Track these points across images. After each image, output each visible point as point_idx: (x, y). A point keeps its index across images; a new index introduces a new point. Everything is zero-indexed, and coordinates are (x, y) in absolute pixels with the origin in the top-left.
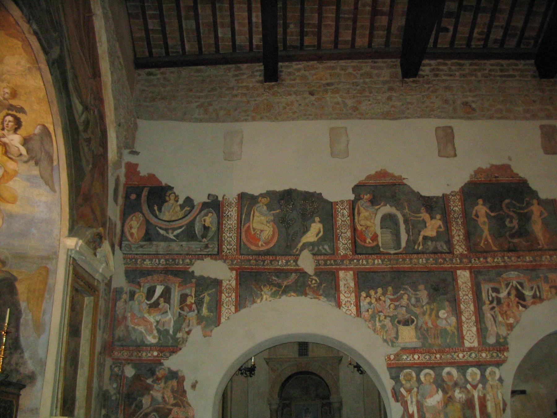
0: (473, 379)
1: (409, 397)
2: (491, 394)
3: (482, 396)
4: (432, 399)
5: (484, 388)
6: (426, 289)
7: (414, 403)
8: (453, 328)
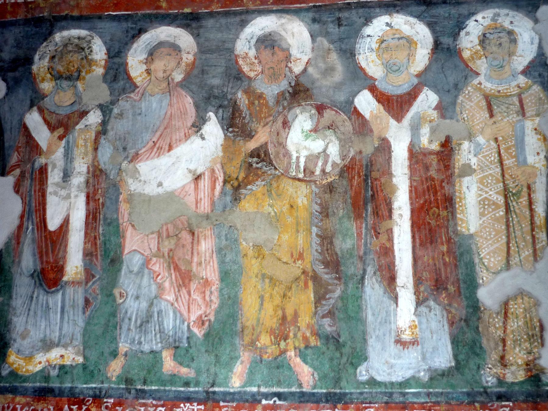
0: (390, 68)
1: (59, 154)
2: (481, 139)
3: (435, 146)
4: (165, 161)
5: (444, 109)
7: (78, 180)
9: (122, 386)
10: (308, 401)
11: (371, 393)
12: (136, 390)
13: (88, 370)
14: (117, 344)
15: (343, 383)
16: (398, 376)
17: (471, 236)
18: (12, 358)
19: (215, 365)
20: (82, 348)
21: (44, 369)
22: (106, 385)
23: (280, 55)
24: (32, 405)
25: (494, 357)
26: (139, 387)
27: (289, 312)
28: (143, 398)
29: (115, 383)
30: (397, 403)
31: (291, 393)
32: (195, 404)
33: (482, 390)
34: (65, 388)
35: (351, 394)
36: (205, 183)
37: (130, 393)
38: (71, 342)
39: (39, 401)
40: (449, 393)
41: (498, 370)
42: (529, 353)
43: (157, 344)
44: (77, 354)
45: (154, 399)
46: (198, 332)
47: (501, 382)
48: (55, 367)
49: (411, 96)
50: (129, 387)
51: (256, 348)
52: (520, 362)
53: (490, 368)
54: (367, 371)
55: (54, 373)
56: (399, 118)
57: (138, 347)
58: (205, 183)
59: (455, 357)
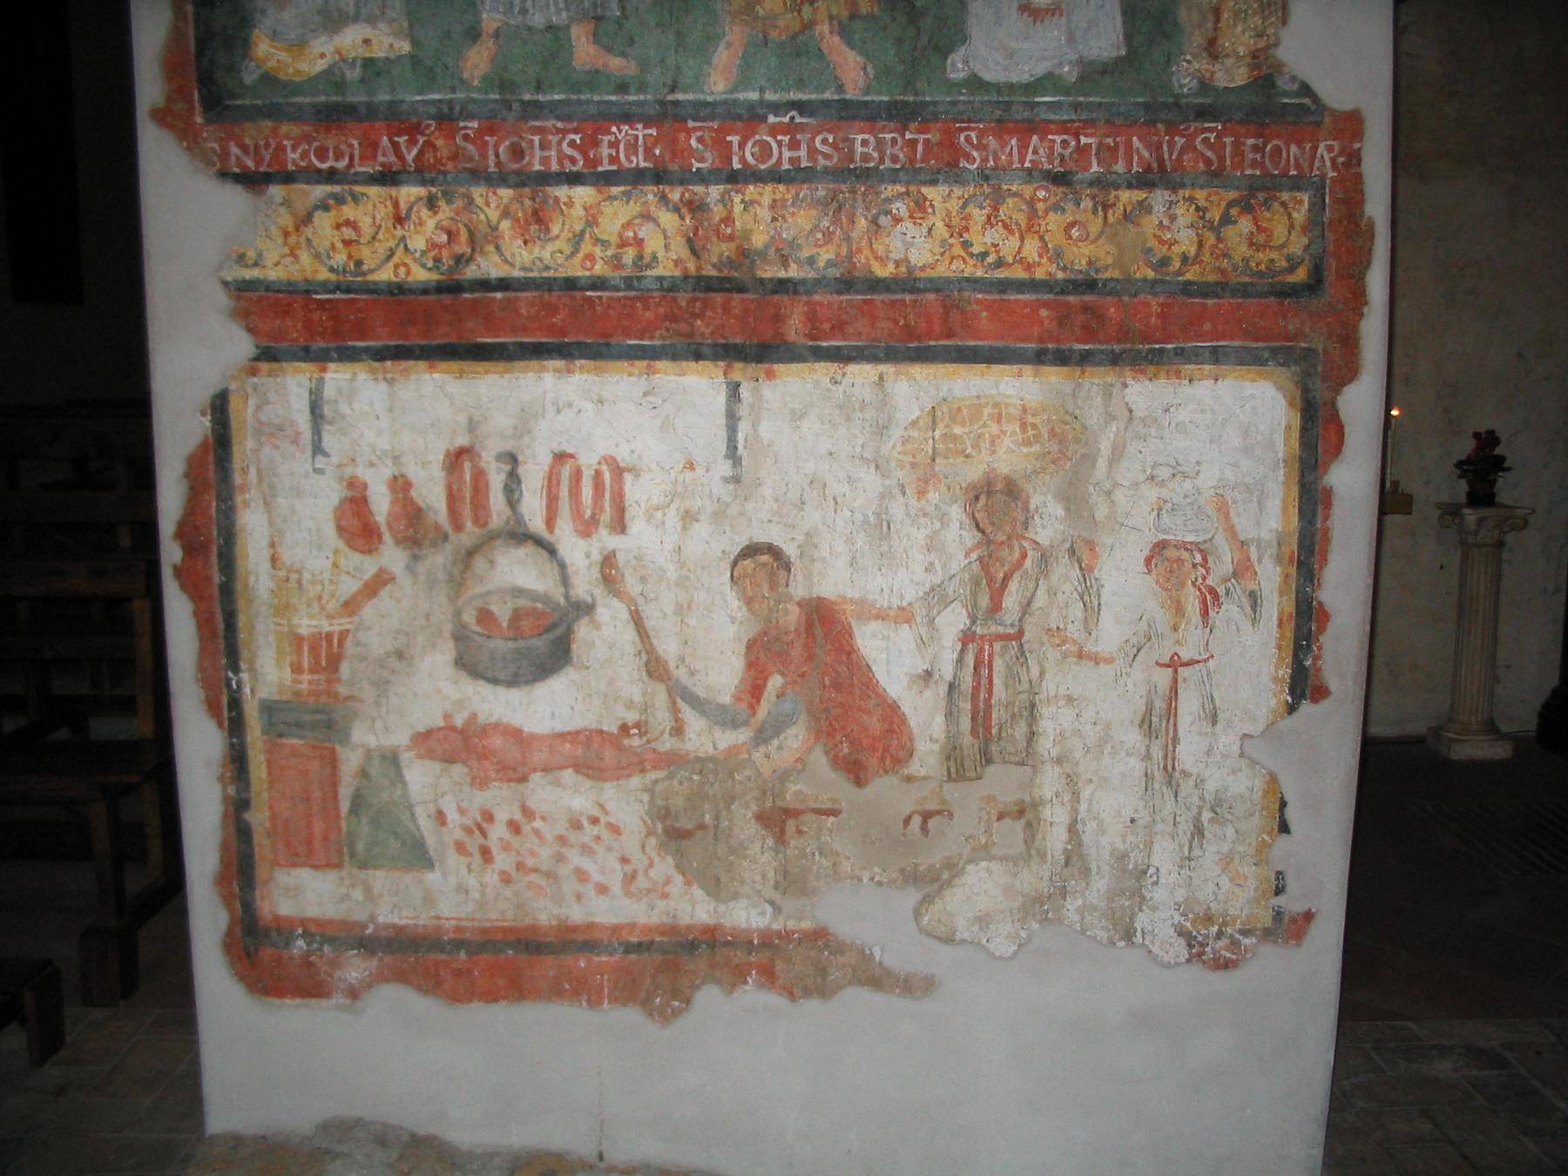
9: (492, 96)
10: (854, 118)
11: (970, 102)
12: (522, 102)
14: (477, 14)
15: (921, 85)
16: (1022, 74)
19: (676, 52)
20: (406, 24)
21: (331, 67)
22: (461, 95)
24: (315, 139)
25: (1198, 40)
26: (527, 97)
28: (537, 118)
29: (478, 90)
30: (1018, 122)
31: (822, 102)
32: (640, 126)
33: (1171, 100)
34: (381, 103)
35: (935, 103)
37: (510, 108)
38: (383, 13)
39: (328, 130)
40: (1112, 104)
41: (1202, 65)
42: (1260, 35)
43: (558, 12)
44: (397, 35)
45: (559, 118)
47: (1205, 86)
48: (353, 64)
50: (508, 97)
51: (756, 19)
52: (1241, 51)
53: (1188, 62)
54: (966, 62)
55: (353, 74)
57: (520, 19)
59: (1128, 38)
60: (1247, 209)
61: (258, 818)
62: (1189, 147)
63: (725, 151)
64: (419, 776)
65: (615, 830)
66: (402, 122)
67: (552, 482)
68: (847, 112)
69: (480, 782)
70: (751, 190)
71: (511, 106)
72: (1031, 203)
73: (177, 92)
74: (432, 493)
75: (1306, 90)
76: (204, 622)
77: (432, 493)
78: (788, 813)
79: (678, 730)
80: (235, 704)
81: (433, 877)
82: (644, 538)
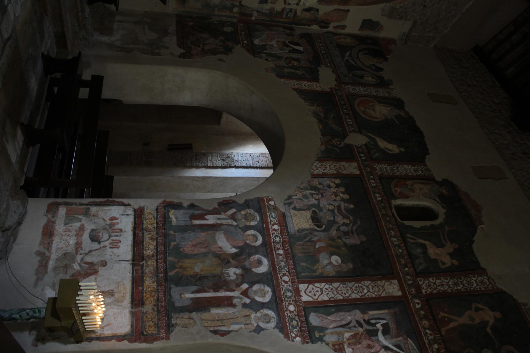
4: (224, 240)
6: (362, 242)
7: (219, 222)
8: (320, 271)
13: (171, 227)
17: (210, 311)
18: (173, 211)
23: (257, 266)
27: (187, 269)
36: (219, 249)
46: (181, 250)
49: (248, 297)
55: (170, 220)
56: (241, 294)
58: (219, 249)
60: (154, 325)
61: (74, 206)
62: (163, 316)
63: (161, 259)
64: (78, 224)
65: (67, 247)
66: (164, 224)
67: (118, 240)
68: (166, 272)
69: (76, 231)
70: (155, 262)
71: (165, 235)
72: (154, 296)
73: (168, 202)
74: (117, 227)
75: (172, 331)
76: (101, 202)
77: (117, 227)
78: (67, 268)
79: (81, 254)
80: (90, 205)
81: (63, 225)
82: (109, 251)
